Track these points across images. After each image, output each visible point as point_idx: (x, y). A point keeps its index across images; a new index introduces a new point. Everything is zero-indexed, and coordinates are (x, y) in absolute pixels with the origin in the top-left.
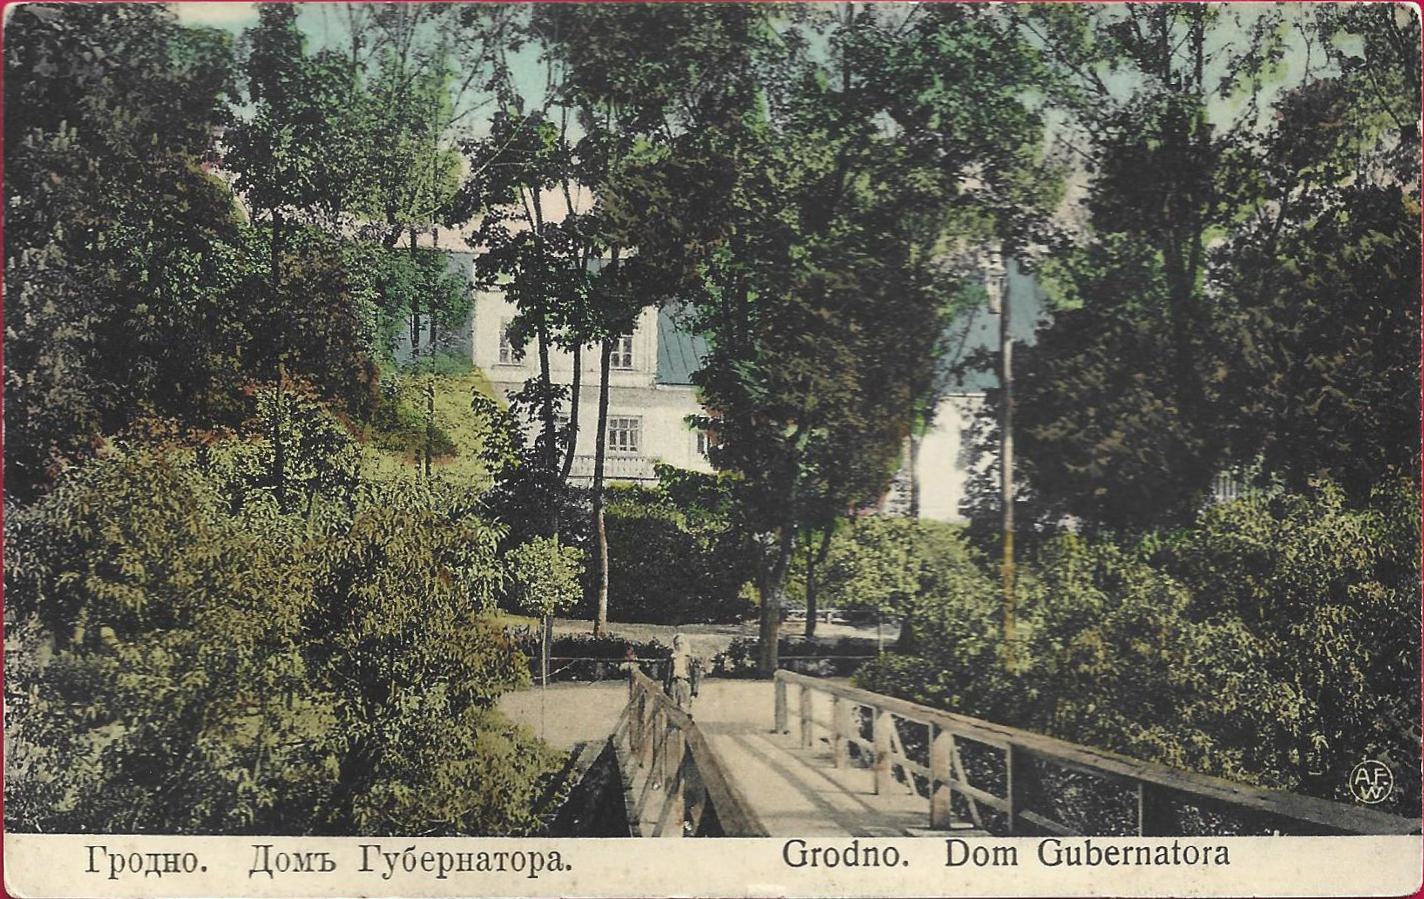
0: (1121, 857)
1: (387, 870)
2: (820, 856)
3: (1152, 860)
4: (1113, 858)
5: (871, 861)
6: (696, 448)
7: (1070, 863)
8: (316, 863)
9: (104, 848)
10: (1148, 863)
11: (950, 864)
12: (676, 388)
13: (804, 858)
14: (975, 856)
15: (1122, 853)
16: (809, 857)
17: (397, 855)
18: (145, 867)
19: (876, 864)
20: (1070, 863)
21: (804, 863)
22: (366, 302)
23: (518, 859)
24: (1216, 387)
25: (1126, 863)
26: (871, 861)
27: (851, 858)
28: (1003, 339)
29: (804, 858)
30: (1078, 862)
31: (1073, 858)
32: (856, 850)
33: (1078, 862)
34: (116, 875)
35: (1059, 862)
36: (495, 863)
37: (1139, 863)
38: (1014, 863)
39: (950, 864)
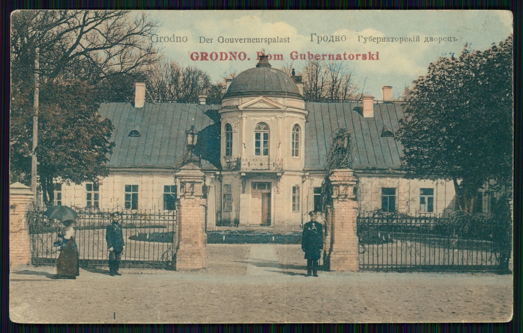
0: (243, 41)
1: (365, 41)
2: (162, 39)
3: (279, 41)
4: (208, 41)
5: (179, 40)
6: (72, 281)
7: (231, 42)
8: (452, 40)
9: (315, 34)
10: (180, 41)
11: (200, 42)
12: (214, 195)
13: (157, 40)
14: (324, 39)
15: (243, 40)
16: (159, 39)
17: (367, 38)
18: (329, 40)
19: (180, 41)
20: (231, 42)
21: (157, 41)
22: (242, 160)
23: (397, 39)
24: (434, 137)
25: (245, 42)
26: (179, 40)
27: (172, 40)
28: (195, 196)
29: (157, 40)
30: (259, 42)
31: (232, 41)
32: (174, 37)
33: (259, 42)
34: (319, 42)
35: (223, 42)
36: (391, 40)
37: (177, 41)
38: (419, 41)
39: (200, 42)
